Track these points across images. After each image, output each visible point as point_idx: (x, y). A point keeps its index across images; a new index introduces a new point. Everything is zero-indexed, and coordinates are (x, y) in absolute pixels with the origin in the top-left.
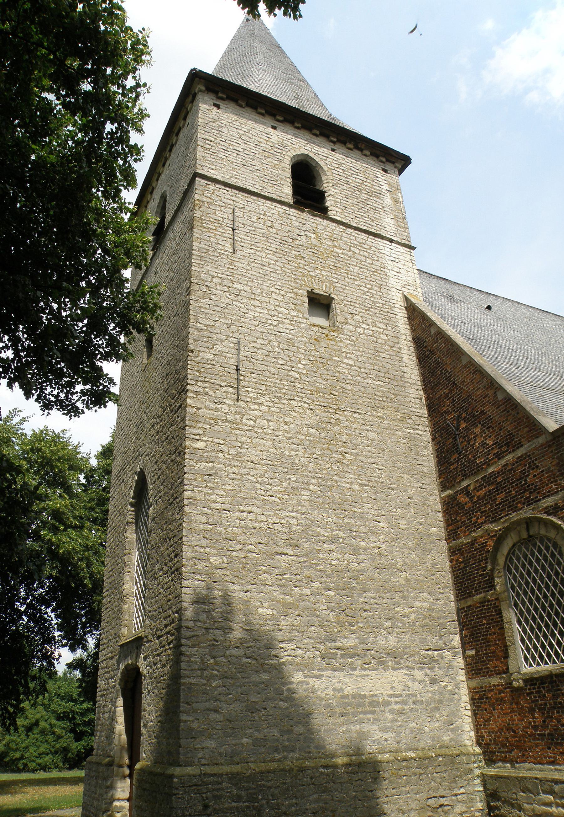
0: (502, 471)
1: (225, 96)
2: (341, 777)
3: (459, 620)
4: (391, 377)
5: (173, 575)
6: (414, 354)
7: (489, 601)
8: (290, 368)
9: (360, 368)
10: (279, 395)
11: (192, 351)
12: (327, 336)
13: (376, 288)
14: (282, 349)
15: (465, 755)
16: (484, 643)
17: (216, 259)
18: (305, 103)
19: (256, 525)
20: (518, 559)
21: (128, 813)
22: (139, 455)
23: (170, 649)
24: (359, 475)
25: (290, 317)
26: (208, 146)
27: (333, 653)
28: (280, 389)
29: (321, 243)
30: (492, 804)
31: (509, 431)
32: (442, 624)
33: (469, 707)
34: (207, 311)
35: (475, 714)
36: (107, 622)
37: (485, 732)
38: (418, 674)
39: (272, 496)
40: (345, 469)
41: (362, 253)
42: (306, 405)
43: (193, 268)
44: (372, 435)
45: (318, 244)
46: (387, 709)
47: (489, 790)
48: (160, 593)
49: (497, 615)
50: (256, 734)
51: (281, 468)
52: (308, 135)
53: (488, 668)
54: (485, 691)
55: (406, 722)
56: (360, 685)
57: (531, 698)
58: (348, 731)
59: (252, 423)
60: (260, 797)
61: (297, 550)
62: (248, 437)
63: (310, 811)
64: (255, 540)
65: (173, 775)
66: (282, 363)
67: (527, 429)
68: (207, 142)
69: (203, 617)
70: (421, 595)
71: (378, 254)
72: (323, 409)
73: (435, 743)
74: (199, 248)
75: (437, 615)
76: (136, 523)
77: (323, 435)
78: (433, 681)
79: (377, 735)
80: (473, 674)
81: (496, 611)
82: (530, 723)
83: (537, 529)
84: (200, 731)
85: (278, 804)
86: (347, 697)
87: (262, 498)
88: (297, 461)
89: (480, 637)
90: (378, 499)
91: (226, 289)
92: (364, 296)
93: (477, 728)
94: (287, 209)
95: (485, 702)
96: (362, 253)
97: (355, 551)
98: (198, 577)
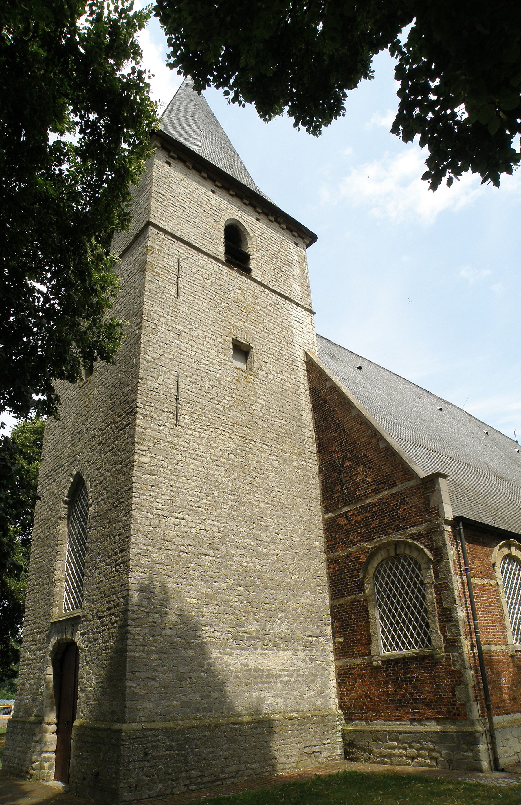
0: (378, 503)
1: (176, 156)
2: (246, 732)
3: (331, 615)
4: (292, 418)
5: (118, 567)
6: (309, 401)
7: (358, 601)
8: (217, 402)
9: (269, 408)
10: (208, 424)
11: (142, 379)
12: (246, 378)
13: (284, 343)
14: (212, 386)
15: (331, 715)
16: (351, 633)
17: (163, 301)
18: (237, 173)
19: (187, 530)
20: (385, 571)
21: (54, 762)
22: (76, 460)
23: (115, 628)
24: (265, 496)
25: (218, 359)
26: (160, 199)
27: (241, 636)
28: (209, 419)
29: (245, 299)
30: (348, 750)
31: (387, 473)
32: (319, 617)
33: (335, 681)
34: (154, 346)
35: (339, 685)
36: (34, 602)
37: (347, 699)
38: (302, 655)
39: (200, 507)
40: (255, 489)
41: (275, 312)
42: (228, 434)
43: (144, 306)
44: (276, 464)
45: (242, 299)
46: (279, 680)
47: (347, 740)
48: (102, 581)
49: (364, 612)
50: (184, 698)
51: (207, 485)
52: (239, 203)
53: (354, 651)
54: (350, 668)
55: (292, 690)
56: (260, 661)
57: (386, 674)
58: (250, 697)
59: (186, 445)
60: (187, 747)
61: (217, 553)
62: (183, 456)
63: (223, 757)
64: (186, 542)
65: (121, 729)
66: (211, 397)
67: (401, 473)
68: (159, 195)
69: (145, 603)
70: (306, 593)
71: (287, 314)
72: (241, 439)
73: (311, 706)
74: (150, 289)
75: (317, 610)
76: (69, 519)
77: (240, 460)
78: (312, 660)
79: (271, 700)
80: (340, 656)
81: (363, 609)
82: (384, 692)
83: (403, 550)
84: (142, 695)
85: (199, 752)
86: (250, 670)
87: (192, 508)
88: (219, 480)
89: (348, 628)
90: (278, 516)
91: (170, 329)
92: (275, 349)
93: (341, 696)
94: (221, 265)
95: (349, 677)
96: (275, 312)
97: (260, 556)
98: (142, 570)
